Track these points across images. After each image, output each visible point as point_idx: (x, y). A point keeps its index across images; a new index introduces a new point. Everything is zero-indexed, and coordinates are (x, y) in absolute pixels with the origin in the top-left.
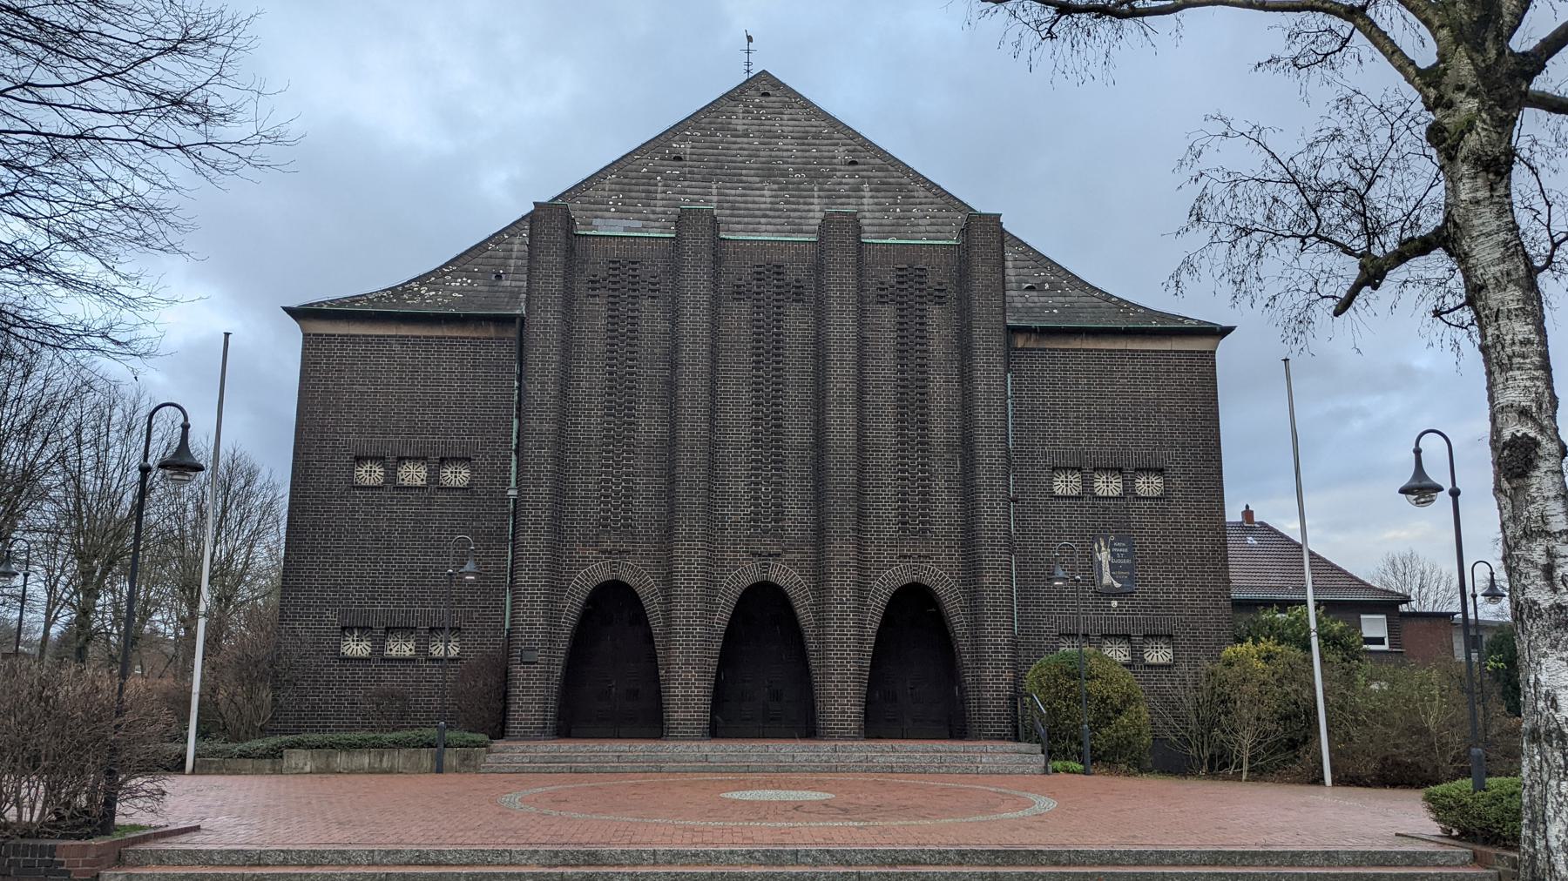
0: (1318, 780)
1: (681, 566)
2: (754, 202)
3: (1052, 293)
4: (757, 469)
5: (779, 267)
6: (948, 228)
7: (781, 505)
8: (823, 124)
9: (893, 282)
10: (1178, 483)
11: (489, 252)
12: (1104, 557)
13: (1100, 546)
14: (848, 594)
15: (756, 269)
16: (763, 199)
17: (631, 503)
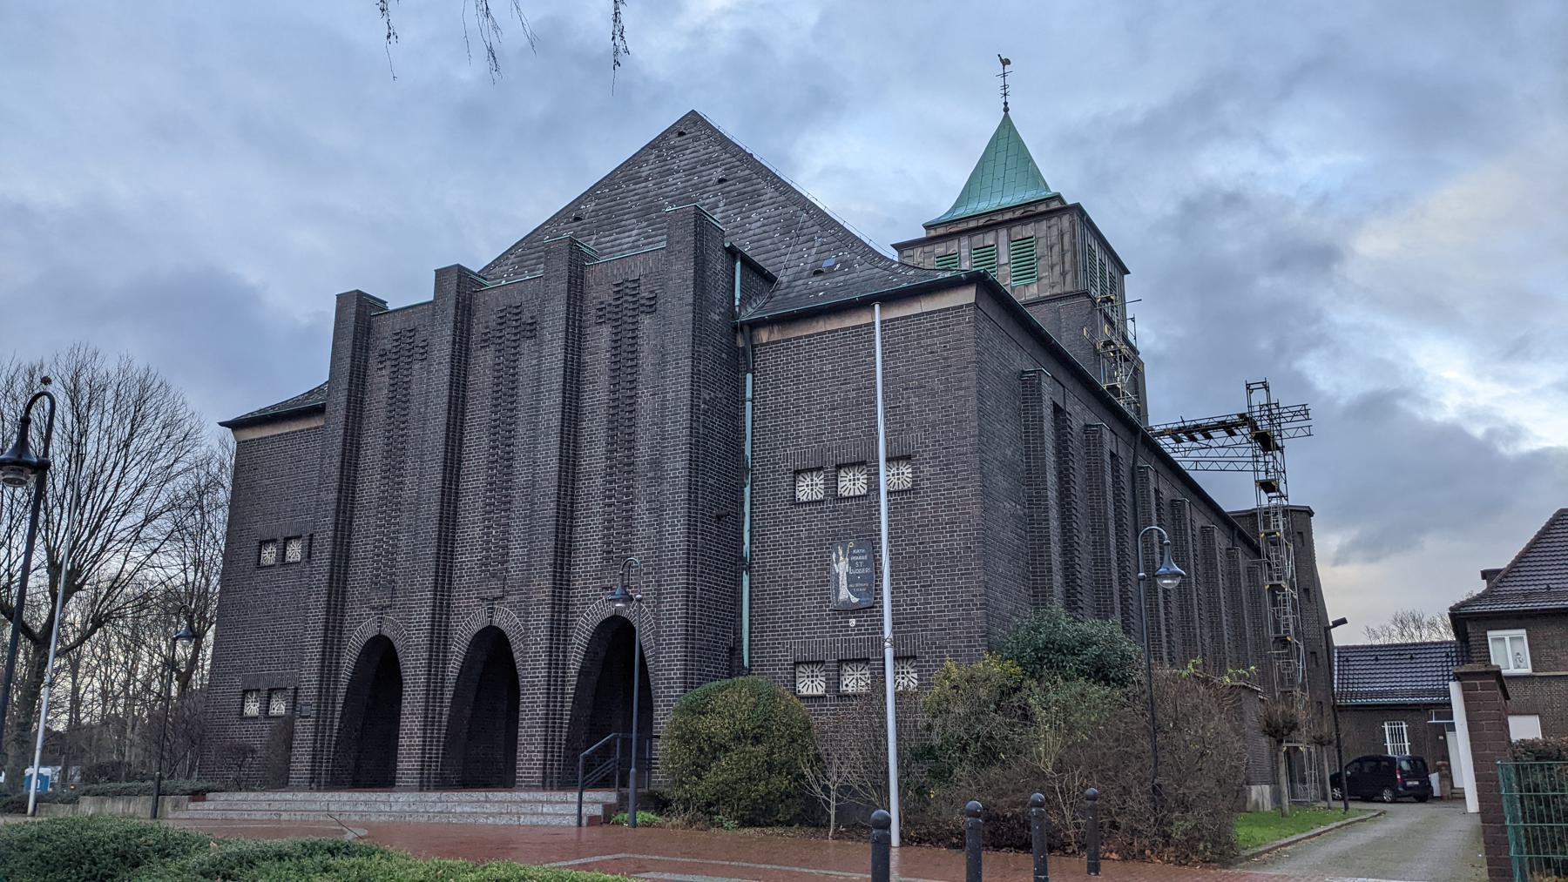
10: (927, 470)
12: (842, 568)
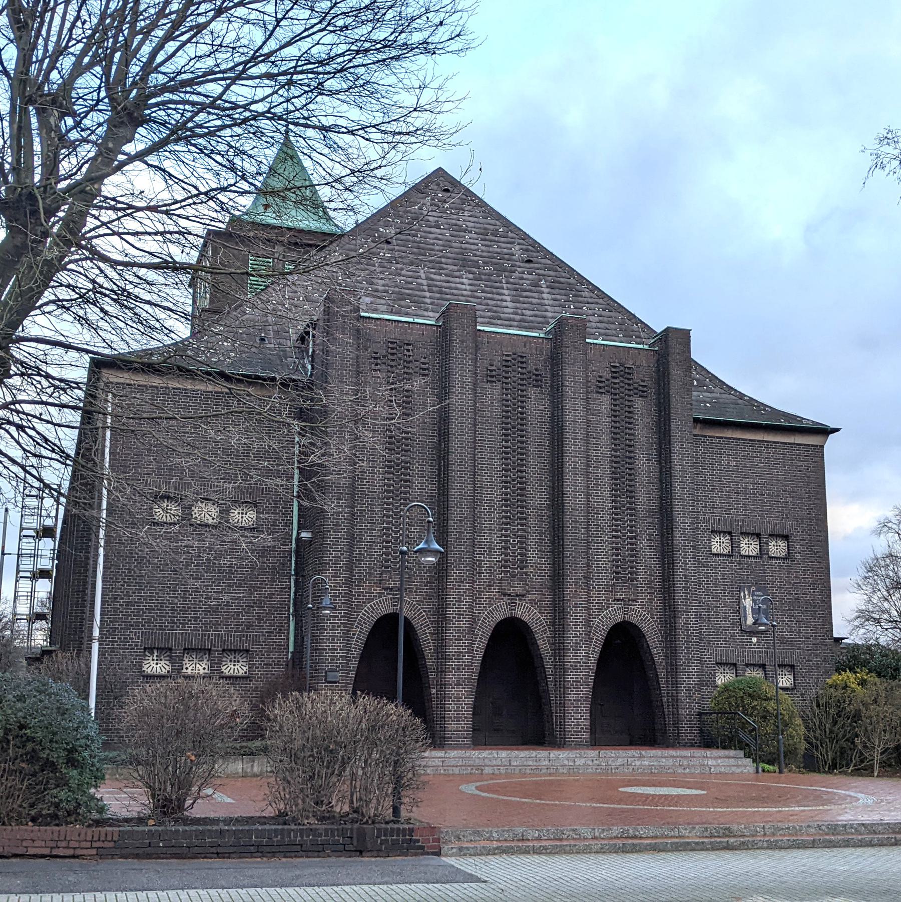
1: (453, 604)
2: (457, 289)
3: (701, 389)
6: (612, 326)
8: (498, 223)
11: (247, 316)
12: (748, 603)
13: (744, 593)
14: (581, 629)
16: (463, 287)
17: (636, 579)
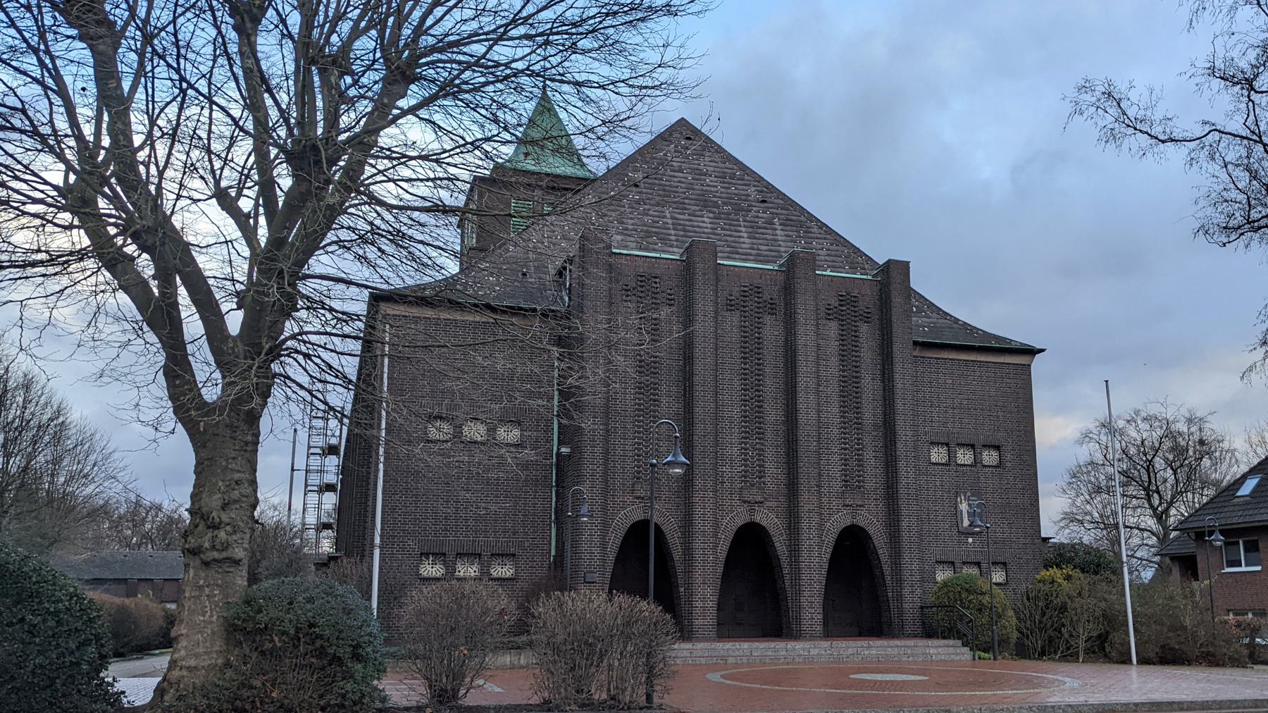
0: (1128, 661)
1: (698, 510)
2: (699, 227)
4: (746, 438)
5: (758, 288)
7: (763, 466)
9: (836, 305)
11: (511, 253)
12: (964, 507)
13: (961, 500)
15: (743, 289)
16: (705, 225)
